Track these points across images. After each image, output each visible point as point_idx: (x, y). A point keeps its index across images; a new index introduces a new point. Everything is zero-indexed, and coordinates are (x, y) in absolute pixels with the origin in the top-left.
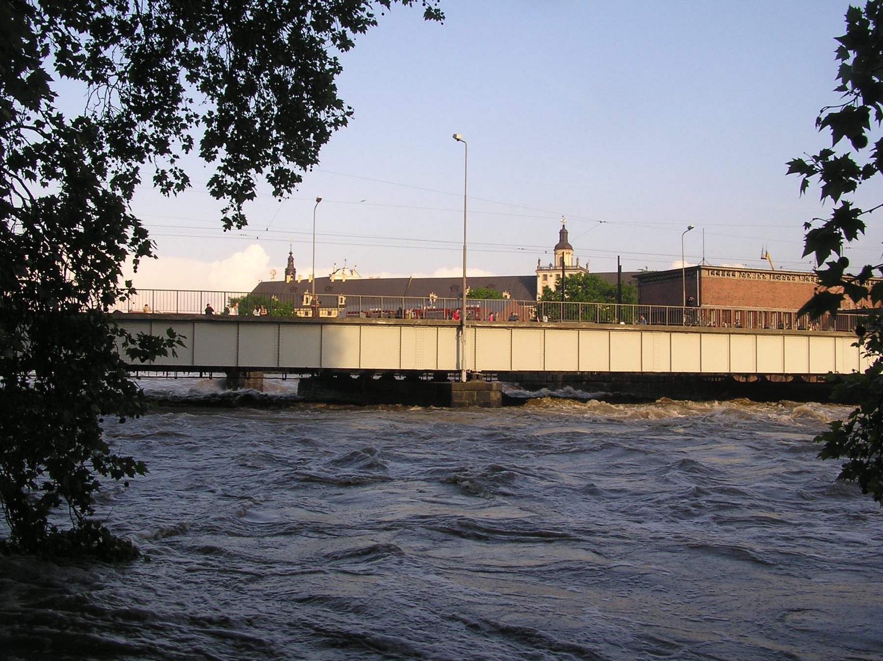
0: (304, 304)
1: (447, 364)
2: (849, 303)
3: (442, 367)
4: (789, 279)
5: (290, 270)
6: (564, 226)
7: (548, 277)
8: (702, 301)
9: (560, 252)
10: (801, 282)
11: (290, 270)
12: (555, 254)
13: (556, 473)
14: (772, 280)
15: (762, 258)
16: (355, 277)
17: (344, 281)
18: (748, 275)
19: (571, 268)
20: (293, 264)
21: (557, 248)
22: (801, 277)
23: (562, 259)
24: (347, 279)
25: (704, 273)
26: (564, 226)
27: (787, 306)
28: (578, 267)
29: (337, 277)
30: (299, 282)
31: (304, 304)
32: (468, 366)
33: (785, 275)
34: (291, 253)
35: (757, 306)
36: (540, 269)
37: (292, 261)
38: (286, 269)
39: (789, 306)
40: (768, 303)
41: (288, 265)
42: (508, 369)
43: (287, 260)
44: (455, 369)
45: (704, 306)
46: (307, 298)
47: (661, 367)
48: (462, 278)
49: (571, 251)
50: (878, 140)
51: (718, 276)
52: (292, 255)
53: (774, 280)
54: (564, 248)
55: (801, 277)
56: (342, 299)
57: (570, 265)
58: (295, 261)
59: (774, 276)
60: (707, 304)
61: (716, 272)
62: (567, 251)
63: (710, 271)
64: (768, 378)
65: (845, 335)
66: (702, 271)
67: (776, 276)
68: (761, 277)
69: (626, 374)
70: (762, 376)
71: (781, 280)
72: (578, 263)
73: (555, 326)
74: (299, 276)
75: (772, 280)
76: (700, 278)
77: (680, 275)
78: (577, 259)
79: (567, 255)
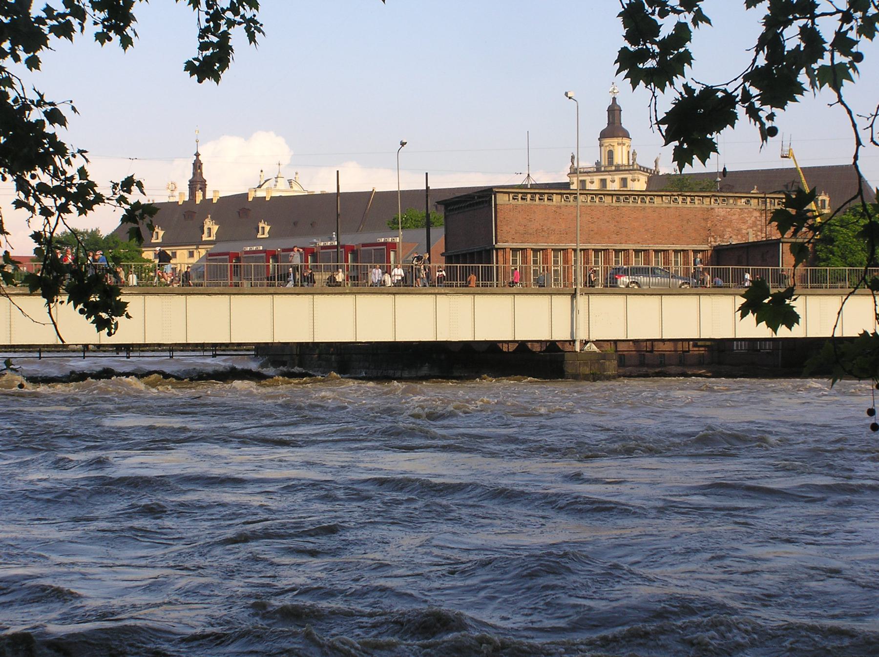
0: (205, 237)
1: (561, 334)
2: (748, 234)
3: (556, 337)
4: (643, 201)
5: (197, 183)
6: (614, 99)
7: (629, 181)
8: (498, 238)
9: (607, 141)
10: (664, 205)
11: (197, 183)
12: (601, 146)
13: (631, 528)
14: (615, 204)
15: (783, 157)
16: (296, 191)
17: (268, 199)
18: (601, 198)
19: (626, 168)
20: (201, 173)
21: (604, 135)
22: (664, 197)
23: (611, 154)
24: (273, 195)
25: (502, 199)
26: (614, 99)
27: (640, 240)
28: (635, 167)
29: (260, 194)
30: (215, 201)
31: (205, 237)
32: (581, 335)
33: (638, 195)
34: (197, 155)
35: (589, 243)
36: (574, 172)
37: (200, 168)
38: (190, 181)
39: (645, 241)
40: (609, 238)
41: (194, 174)
42: (472, 339)
43: (192, 166)
44: (569, 338)
45: (500, 245)
46: (209, 229)
47: (384, 335)
48: (397, 191)
49: (625, 140)
50: (704, 13)
51: (523, 202)
52: (200, 158)
53: (618, 204)
54: (613, 136)
55: (664, 197)
56: (263, 228)
57: (625, 162)
58: (204, 167)
59: (618, 198)
60: (507, 242)
61: (520, 195)
62: (620, 140)
63: (511, 196)
64: (529, 345)
65: (447, 292)
66: (498, 195)
67: (622, 198)
68: (597, 200)
69: (310, 344)
70: (523, 344)
71: (631, 204)
72: (634, 160)
73: (21, 292)
74: (215, 191)
75: (615, 204)
76: (496, 204)
77: (487, 199)
78: (634, 154)
79: (620, 147)
